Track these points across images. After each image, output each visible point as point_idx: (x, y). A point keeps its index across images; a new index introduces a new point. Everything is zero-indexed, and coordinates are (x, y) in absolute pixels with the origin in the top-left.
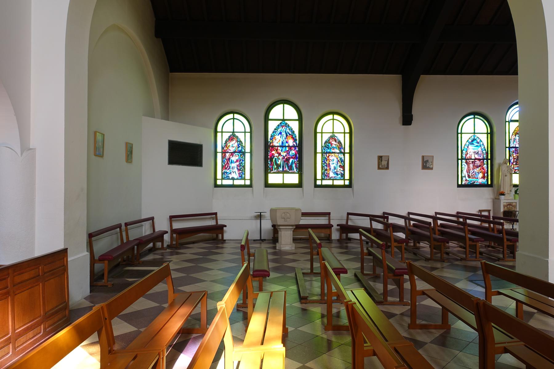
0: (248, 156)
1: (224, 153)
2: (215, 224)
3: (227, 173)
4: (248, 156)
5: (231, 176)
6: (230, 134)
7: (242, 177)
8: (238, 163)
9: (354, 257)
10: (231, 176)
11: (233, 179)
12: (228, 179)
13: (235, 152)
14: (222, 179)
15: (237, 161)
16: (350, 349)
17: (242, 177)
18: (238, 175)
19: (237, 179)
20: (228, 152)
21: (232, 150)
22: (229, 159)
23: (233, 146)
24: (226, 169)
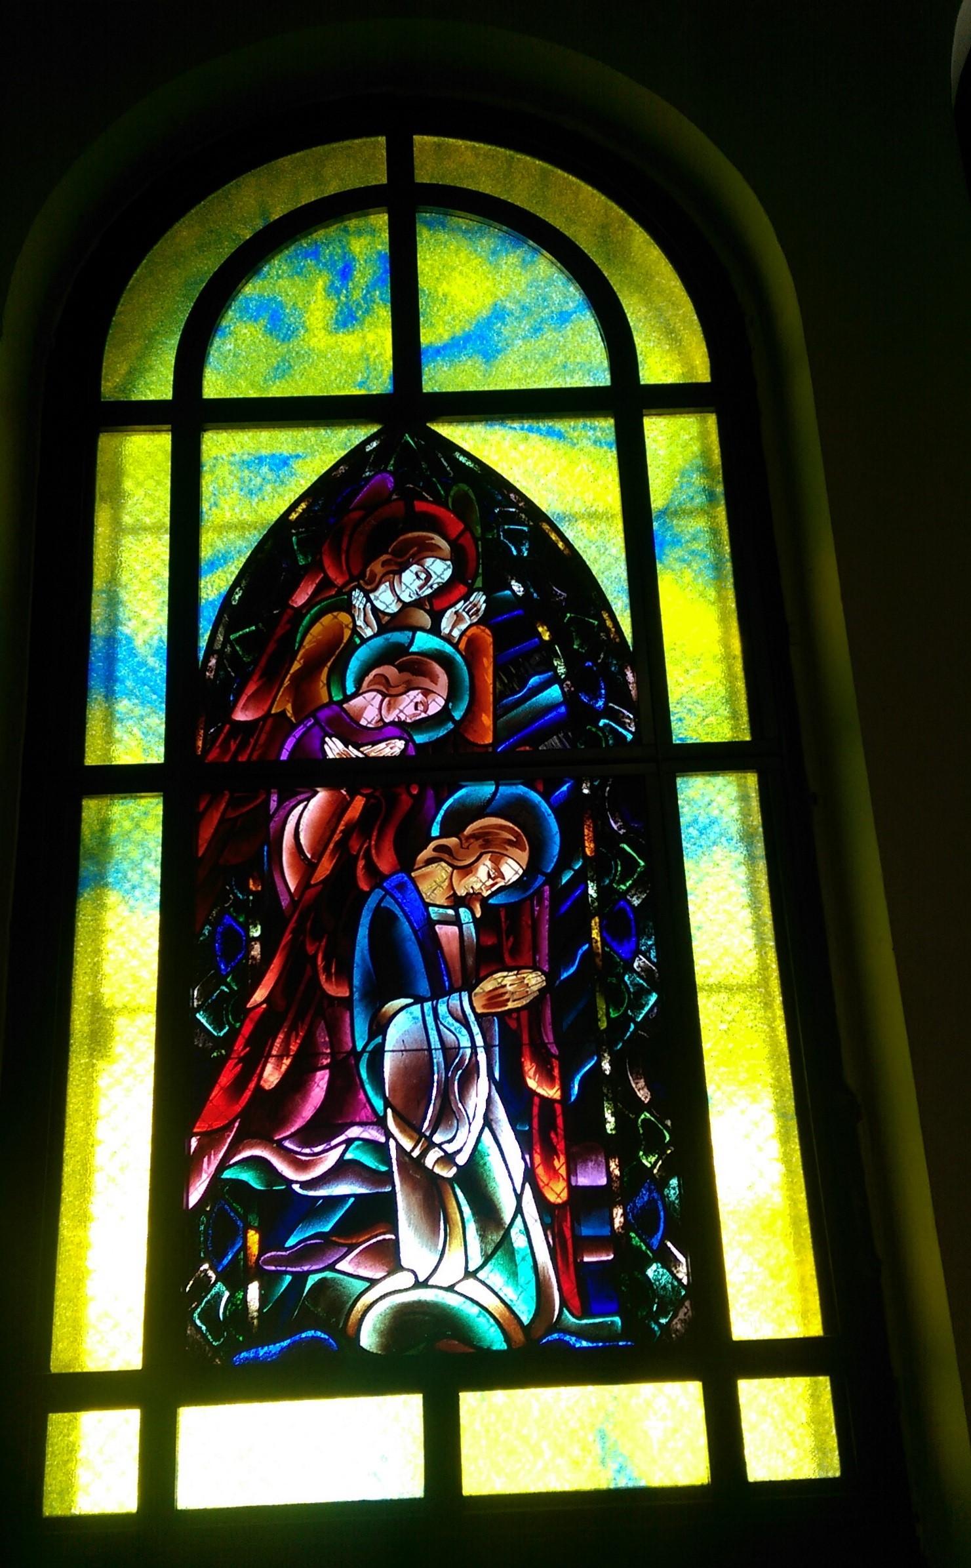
0: (717, 821)
1: (214, 789)
2: (407, 1482)
3: (281, 1208)
4: (717, 821)
5: (376, 1303)
6: (320, 451)
7: (635, 1302)
8: (519, 985)
9: (629, 640)
10: (376, 1303)
11: (436, 1361)
12: (313, 1355)
13: (442, 760)
14: (191, 1360)
15: (504, 931)
16: (428, 337)
17: (635, 1302)
18: (532, 1238)
19: (534, 1358)
20: (310, 772)
21: (388, 714)
22: (333, 900)
23: (407, 647)
24: (264, 1117)
